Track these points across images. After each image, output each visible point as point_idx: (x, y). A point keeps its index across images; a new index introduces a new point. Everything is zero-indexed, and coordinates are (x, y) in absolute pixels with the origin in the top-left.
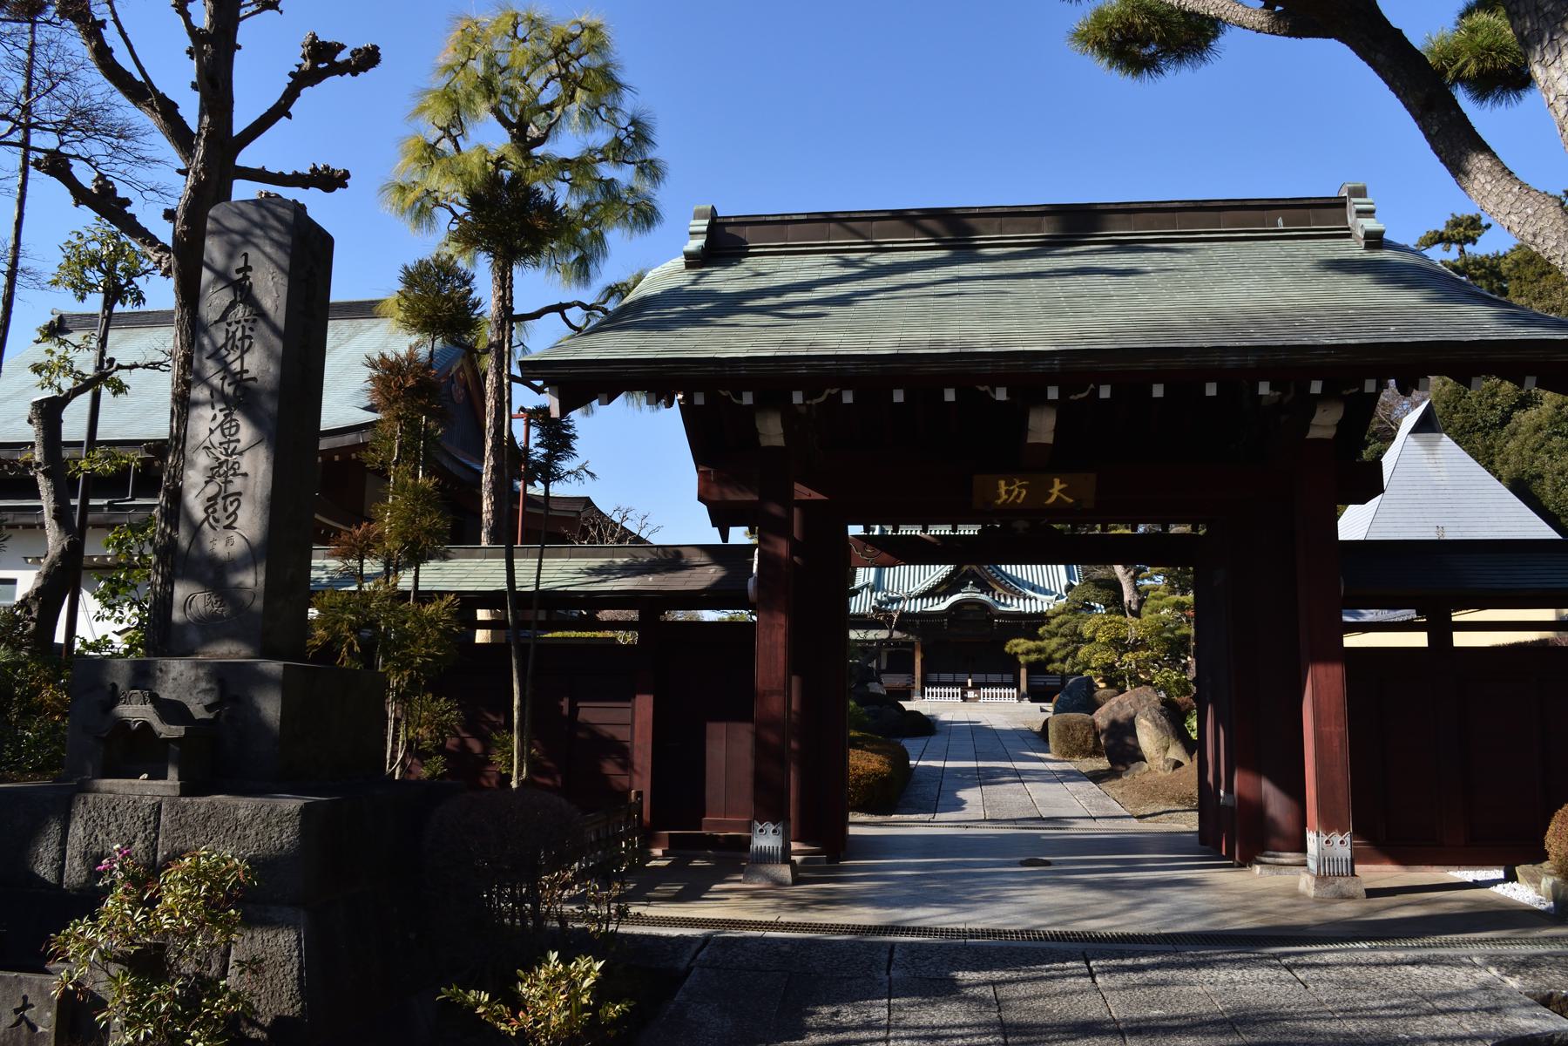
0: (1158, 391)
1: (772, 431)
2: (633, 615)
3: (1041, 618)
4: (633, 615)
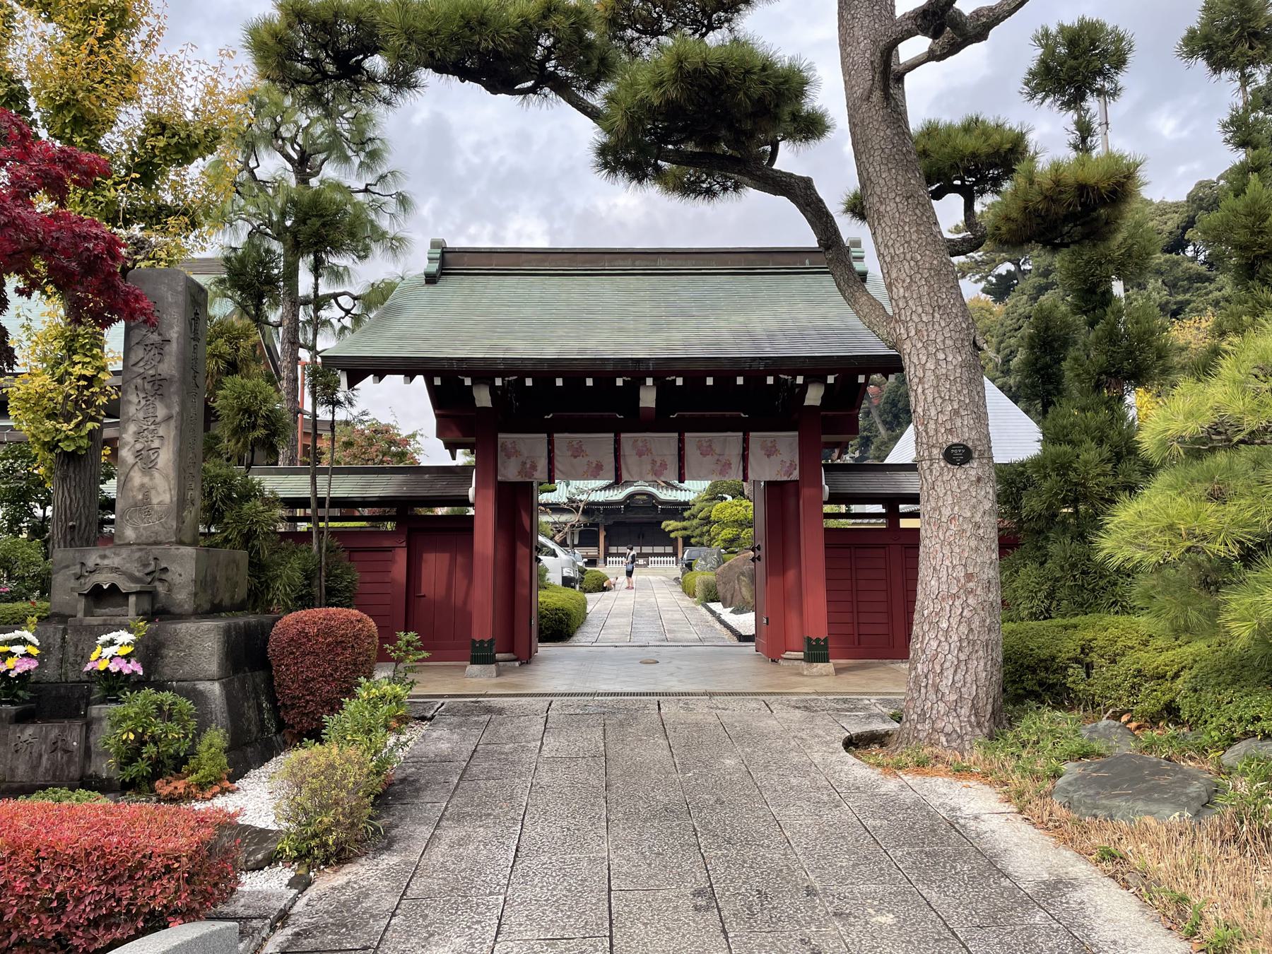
0: (589, 382)
1: (483, 398)
2: (393, 512)
3: (686, 505)
4: (393, 512)
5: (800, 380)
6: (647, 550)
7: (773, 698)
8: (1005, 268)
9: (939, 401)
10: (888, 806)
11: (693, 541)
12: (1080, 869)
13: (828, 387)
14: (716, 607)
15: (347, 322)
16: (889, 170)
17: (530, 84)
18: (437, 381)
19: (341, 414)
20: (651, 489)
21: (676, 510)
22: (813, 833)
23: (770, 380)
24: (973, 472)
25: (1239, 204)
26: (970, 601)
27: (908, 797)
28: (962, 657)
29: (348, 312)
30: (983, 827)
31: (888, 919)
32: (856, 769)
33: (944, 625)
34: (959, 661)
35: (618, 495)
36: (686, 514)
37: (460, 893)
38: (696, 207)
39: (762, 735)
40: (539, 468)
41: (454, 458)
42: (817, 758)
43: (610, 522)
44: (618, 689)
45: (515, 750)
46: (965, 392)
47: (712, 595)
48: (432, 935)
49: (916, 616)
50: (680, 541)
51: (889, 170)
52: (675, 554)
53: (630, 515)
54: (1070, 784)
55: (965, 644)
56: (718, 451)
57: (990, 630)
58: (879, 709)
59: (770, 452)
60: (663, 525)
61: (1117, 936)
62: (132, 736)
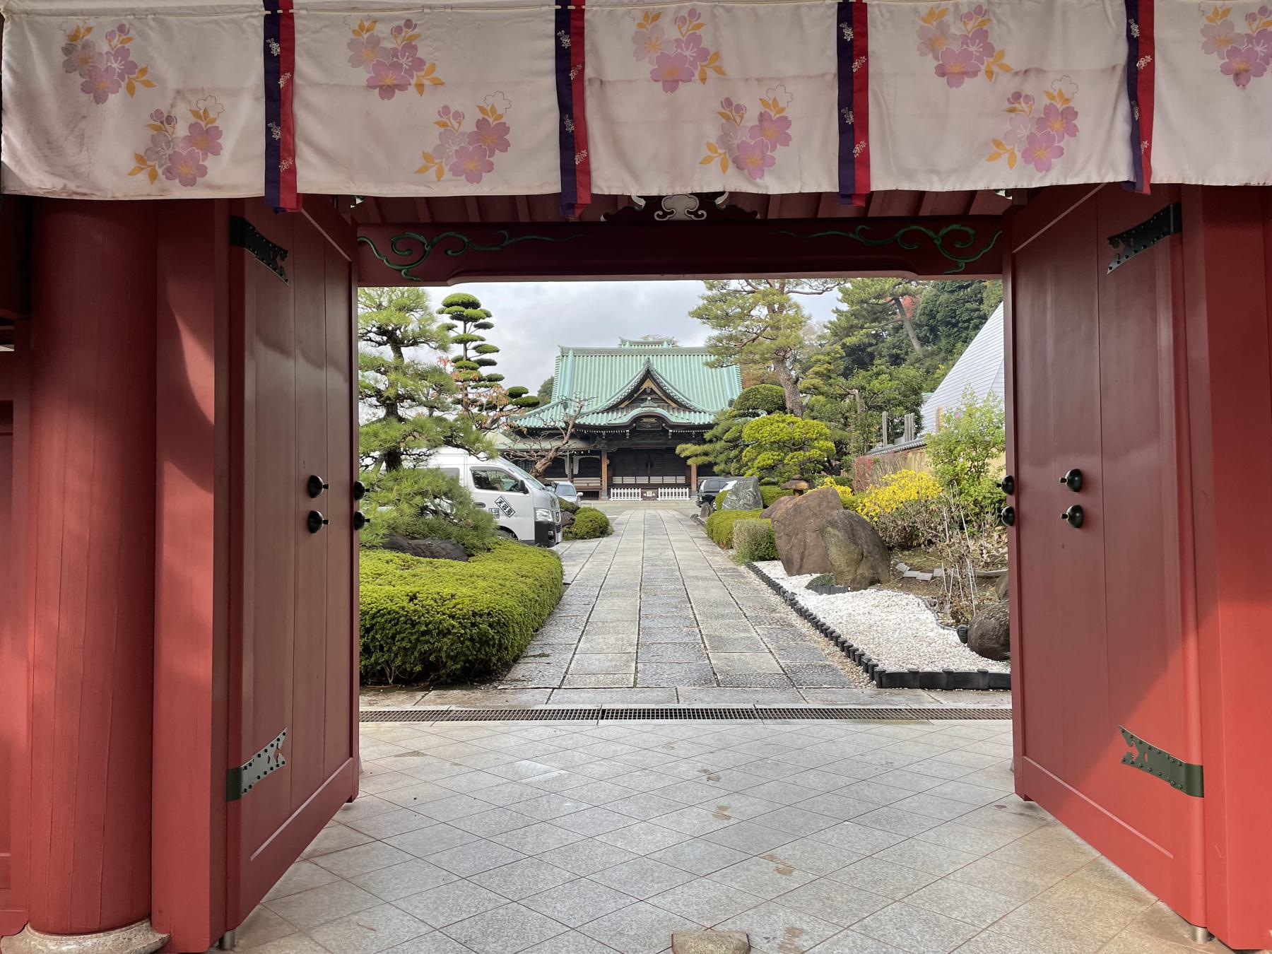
6: (656, 480)
11: (716, 469)
14: (774, 570)
40: (228, 142)
43: (614, 449)
47: (763, 549)
56: (1015, 56)
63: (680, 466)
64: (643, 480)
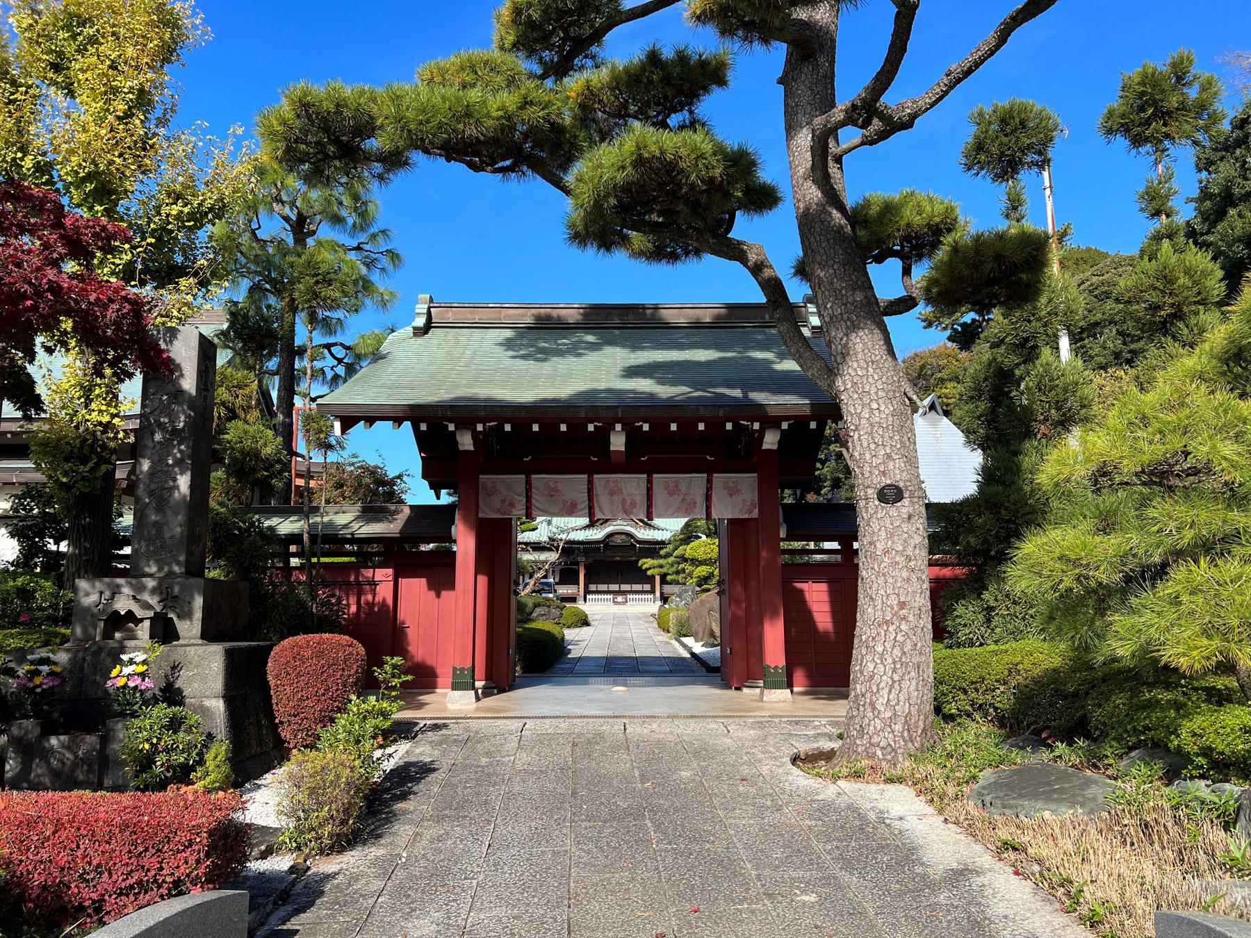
1: (466, 442)
5: (756, 426)
6: (625, 587)
7: (731, 720)
8: (969, 317)
9: (873, 446)
10: (826, 809)
12: (985, 859)
13: (783, 431)
15: (341, 370)
16: (828, 240)
17: (508, 163)
18: (423, 427)
19: (332, 457)
20: (629, 529)
21: (653, 549)
22: (755, 830)
23: (729, 426)
24: (904, 510)
25: (1151, 267)
26: (903, 627)
27: (842, 802)
28: (896, 677)
29: (340, 361)
30: (905, 825)
31: (812, 898)
32: (799, 779)
33: (880, 649)
34: (894, 682)
35: (597, 534)
36: (662, 552)
37: (439, 877)
38: (662, 270)
39: (716, 751)
41: (438, 498)
42: (765, 770)
43: (590, 561)
44: (587, 713)
45: (491, 764)
46: (897, 438)
48: (413, 910)
49: (856, 641)
50: (658, 578)
51: (828, 240)
52: (653, 591)
53: (608, 553)
54: (984, 788)
55: (898, 666)
57: (921, 654)
58: (829, 729)
59: (732, 492)
60: (640, 563)
61: (1010, 912)
62: (147, 746)
63: (643, 577)
64: (614, 587)
